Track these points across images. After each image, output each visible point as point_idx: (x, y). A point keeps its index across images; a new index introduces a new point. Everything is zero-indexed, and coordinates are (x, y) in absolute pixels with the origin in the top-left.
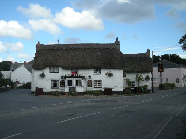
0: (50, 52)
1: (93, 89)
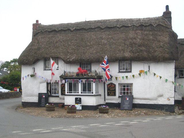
1: (115, 100)
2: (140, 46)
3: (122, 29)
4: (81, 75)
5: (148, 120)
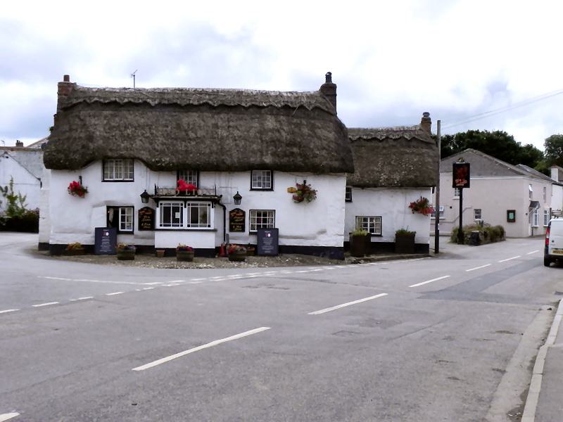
1: (244, 238)
2: (288, 145)
3: (251, 110)
4: (188, 193)
5: (286, 271)
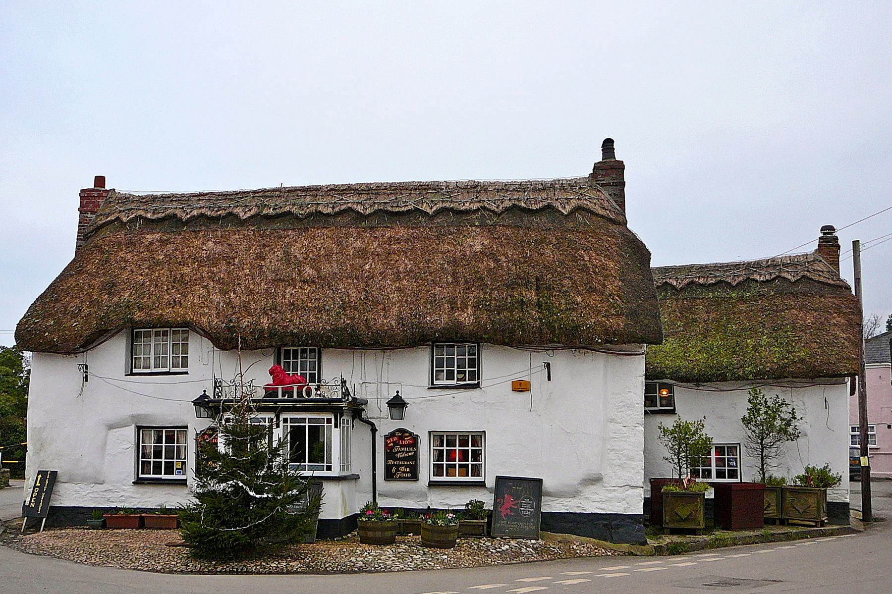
0: (149, 237)
2: (511, 286)
